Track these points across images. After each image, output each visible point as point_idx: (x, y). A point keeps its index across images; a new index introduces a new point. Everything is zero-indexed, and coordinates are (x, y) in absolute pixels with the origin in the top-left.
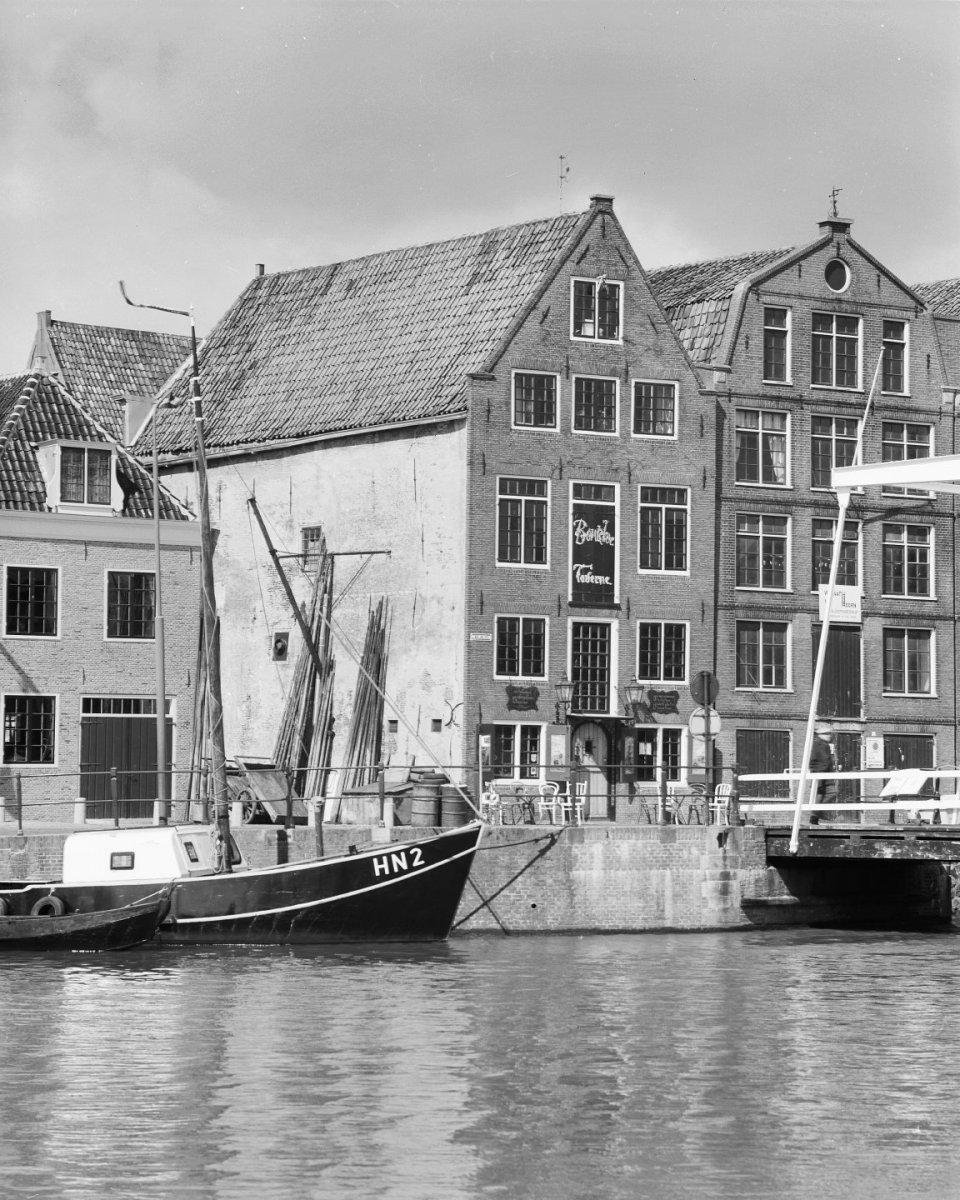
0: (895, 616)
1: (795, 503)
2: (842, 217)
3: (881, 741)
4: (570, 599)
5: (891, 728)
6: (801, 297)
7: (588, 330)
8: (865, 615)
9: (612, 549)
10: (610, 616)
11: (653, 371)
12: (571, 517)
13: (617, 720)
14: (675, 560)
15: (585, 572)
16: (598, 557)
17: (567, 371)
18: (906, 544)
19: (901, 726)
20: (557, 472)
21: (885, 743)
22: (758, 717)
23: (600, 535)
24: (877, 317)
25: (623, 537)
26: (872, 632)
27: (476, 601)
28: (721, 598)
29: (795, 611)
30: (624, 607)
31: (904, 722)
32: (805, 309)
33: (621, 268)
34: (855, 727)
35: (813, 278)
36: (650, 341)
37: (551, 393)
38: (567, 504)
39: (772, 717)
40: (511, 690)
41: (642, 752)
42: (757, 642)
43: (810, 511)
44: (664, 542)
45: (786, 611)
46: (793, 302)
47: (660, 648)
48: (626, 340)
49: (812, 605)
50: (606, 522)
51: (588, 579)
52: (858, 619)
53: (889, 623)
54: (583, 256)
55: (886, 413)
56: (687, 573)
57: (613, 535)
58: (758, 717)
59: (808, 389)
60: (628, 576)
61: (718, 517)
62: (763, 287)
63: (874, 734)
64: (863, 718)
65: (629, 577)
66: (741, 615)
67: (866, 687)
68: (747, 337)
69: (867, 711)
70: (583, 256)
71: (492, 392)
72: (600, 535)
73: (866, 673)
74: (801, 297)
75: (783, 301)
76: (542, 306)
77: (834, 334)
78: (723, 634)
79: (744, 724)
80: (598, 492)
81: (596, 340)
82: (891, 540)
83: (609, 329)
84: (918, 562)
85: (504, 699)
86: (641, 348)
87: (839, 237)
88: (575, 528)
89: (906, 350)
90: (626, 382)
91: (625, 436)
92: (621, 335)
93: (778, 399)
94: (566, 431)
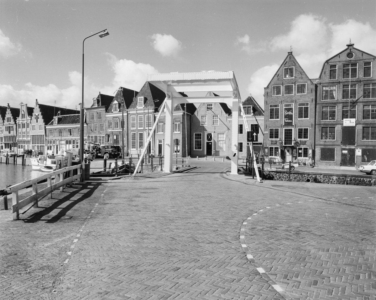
0: (366, 124)
1: (337, 103)
2: (352, 43)
3: (360, 150)
4: (284, 125)
5: (364, 147)
6: (339, 62)
7: (287, 76)
8: (356, 124)
9: (292, 115)
10: (292, 127)
11: (301, 82)
12: (284, 110)
13: (293, 146)
14: (306, 116)
15: (287, 120)
16: (290, 117)
17: (283, 85)
18: (371, 109)
19: (367, 147)
20: (281, 103)
21: (345, 118)
22: (326, 145)
23: (290, 113)
24: (362, 63)
25: (295, 113)
26: (359, 128)
27: (265, 126)
28: (316, 123)
29: (337, 124)
30: (295, 126)
31: (368, 146)
32: (341, 64)
33: (294, 64)
34: (353, 147)
35: (344, 58)
36: (300, 76)
37: (280, 89)
38: (283, 108)
39: (330, 145)
40: (272, 141)
41: (300, 152)
42: (328, 131)
43: (341, 104)
44: (303, 113)
45: (334, 125)
46: (338, 63)
47: (303, 133)
48: (295, 77)
49: (341, 123)
50: (291, 111)
51: (287, 121)
52: (354, 125)
53: (364, 126)
54: (286, 63)
55: (364, 82)
56: (308, 119)
57: (292, 113)
58: (326, 145)
59: (342, 79)
60: (296, 120)
61: (316, 108)
62: (329, 61)
63: (359, 149)
64: (356, 145)
65: (296, 120)
66: (322, 126)
67: (357, 139)
68: (325, 72)
69: (357, 144)
70: (286, 63)
71: (269, 90)
72: (290, 113)
73: (357, 136)
74: (339, 62)
75: (336, 63)
76: (278, 74)
77: (350, 68)
78: (317, 130)
79: (322, 147)
80: (290, 105)
81: (289, 78)
82: (366, 108)
83: (292, 76)
84: (350, 78)
85: (271, 143)
86: (298, 78)
87: (350, 47)
88: (285, 112)
89: (371, 68)
90: (295, 85)
91: (295, 95)
92: (294, 76)
93: (333, 83)
94: (283, 95)
